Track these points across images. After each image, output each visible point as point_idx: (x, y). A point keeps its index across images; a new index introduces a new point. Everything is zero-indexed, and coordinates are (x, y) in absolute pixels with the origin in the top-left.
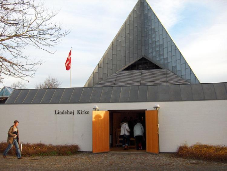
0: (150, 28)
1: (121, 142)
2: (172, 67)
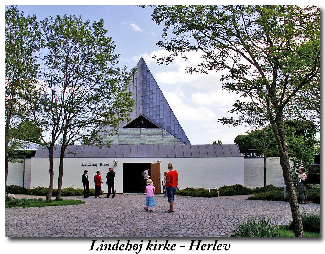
0: (149, 89)
1: (293, 25)
2: (167, 126)
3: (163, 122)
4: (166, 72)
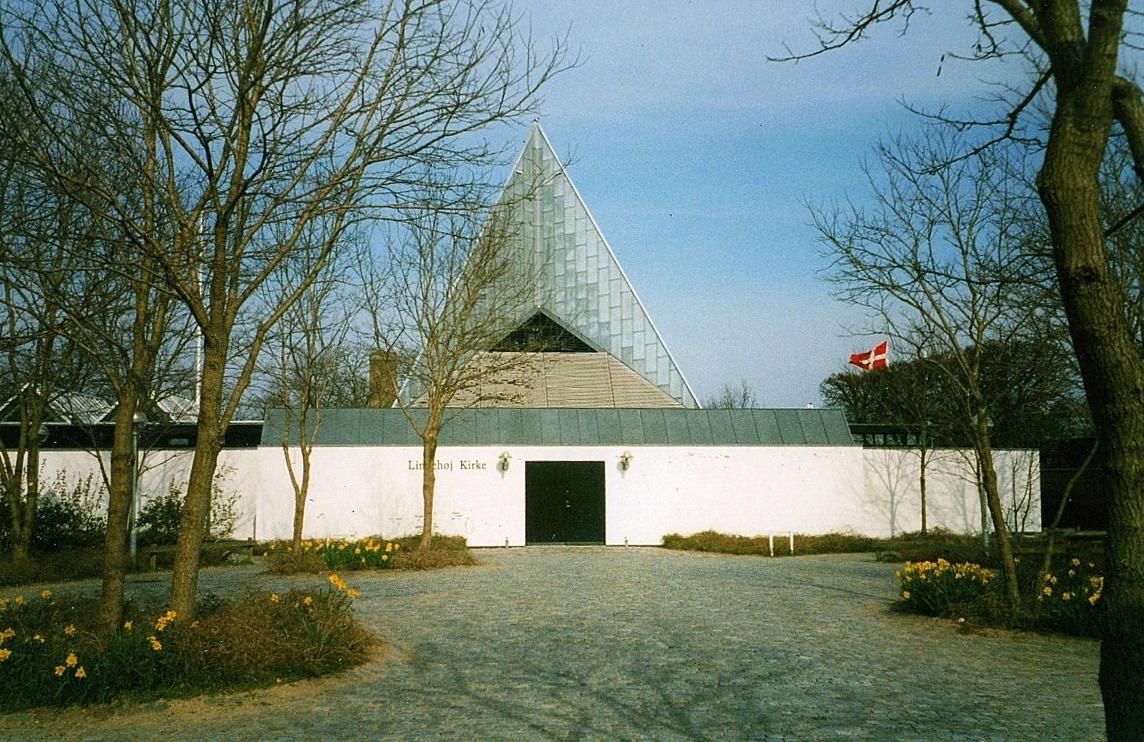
3: (610, 336)
4: (714, 534)
